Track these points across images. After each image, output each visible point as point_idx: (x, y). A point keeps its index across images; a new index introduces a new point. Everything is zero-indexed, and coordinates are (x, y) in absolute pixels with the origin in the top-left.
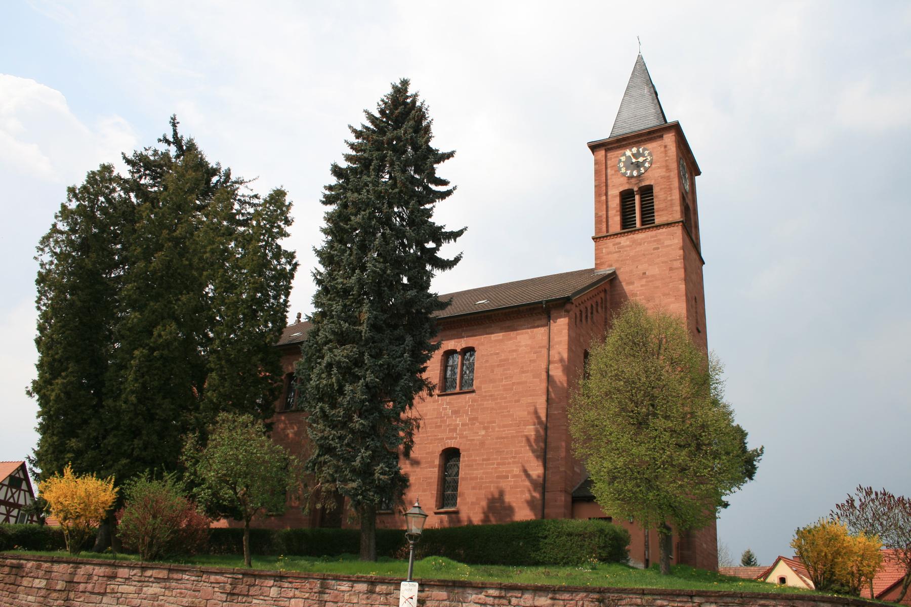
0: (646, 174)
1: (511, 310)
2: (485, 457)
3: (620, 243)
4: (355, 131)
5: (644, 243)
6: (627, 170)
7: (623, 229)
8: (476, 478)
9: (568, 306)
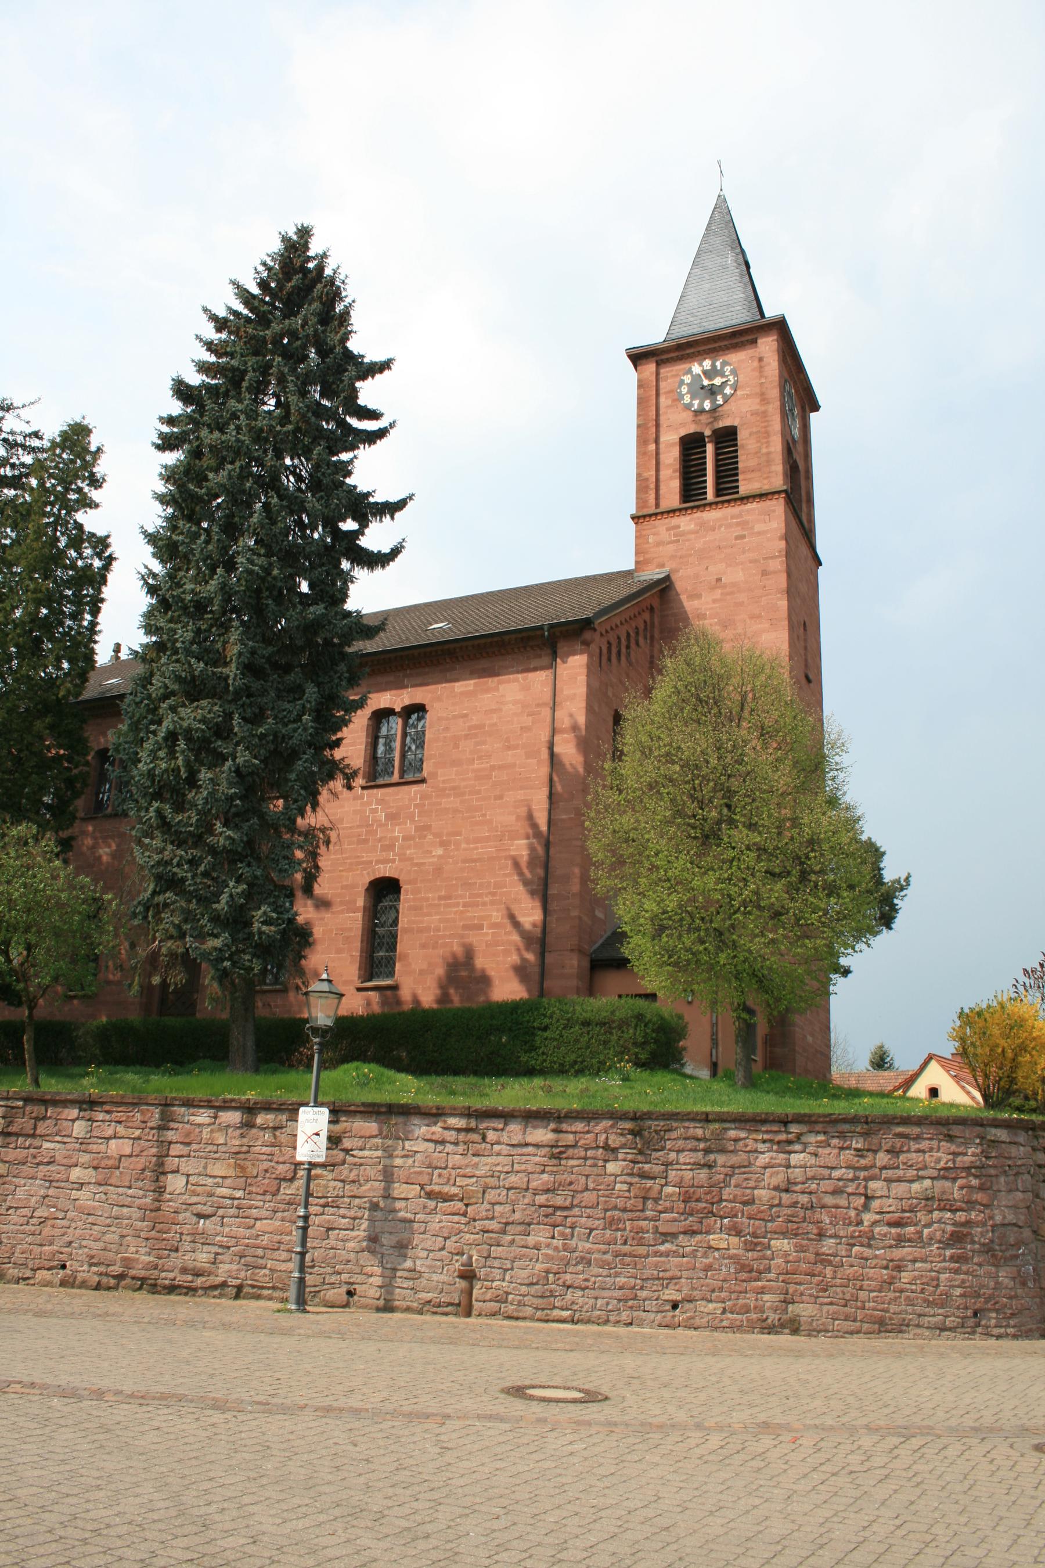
0: (726, 407)
1: (489, 640)
2: (443, 893)
3: (679, 527)
4: (214, 318)
5: (720, 526)
6: (692, 399)
7: (685, 502)
8: (428, 929)
9: (587, 635)
